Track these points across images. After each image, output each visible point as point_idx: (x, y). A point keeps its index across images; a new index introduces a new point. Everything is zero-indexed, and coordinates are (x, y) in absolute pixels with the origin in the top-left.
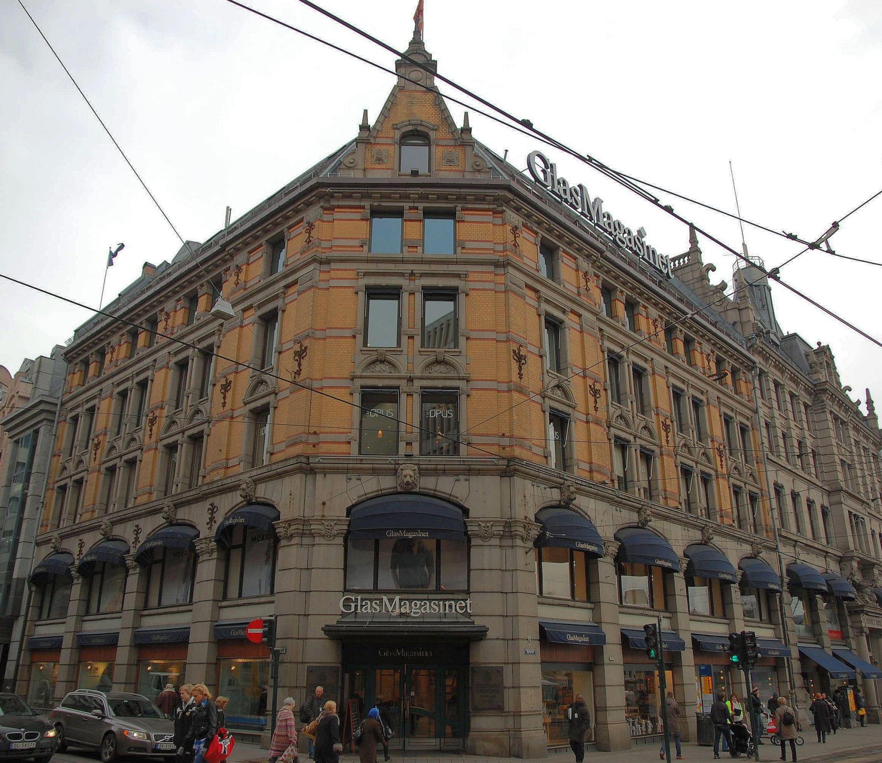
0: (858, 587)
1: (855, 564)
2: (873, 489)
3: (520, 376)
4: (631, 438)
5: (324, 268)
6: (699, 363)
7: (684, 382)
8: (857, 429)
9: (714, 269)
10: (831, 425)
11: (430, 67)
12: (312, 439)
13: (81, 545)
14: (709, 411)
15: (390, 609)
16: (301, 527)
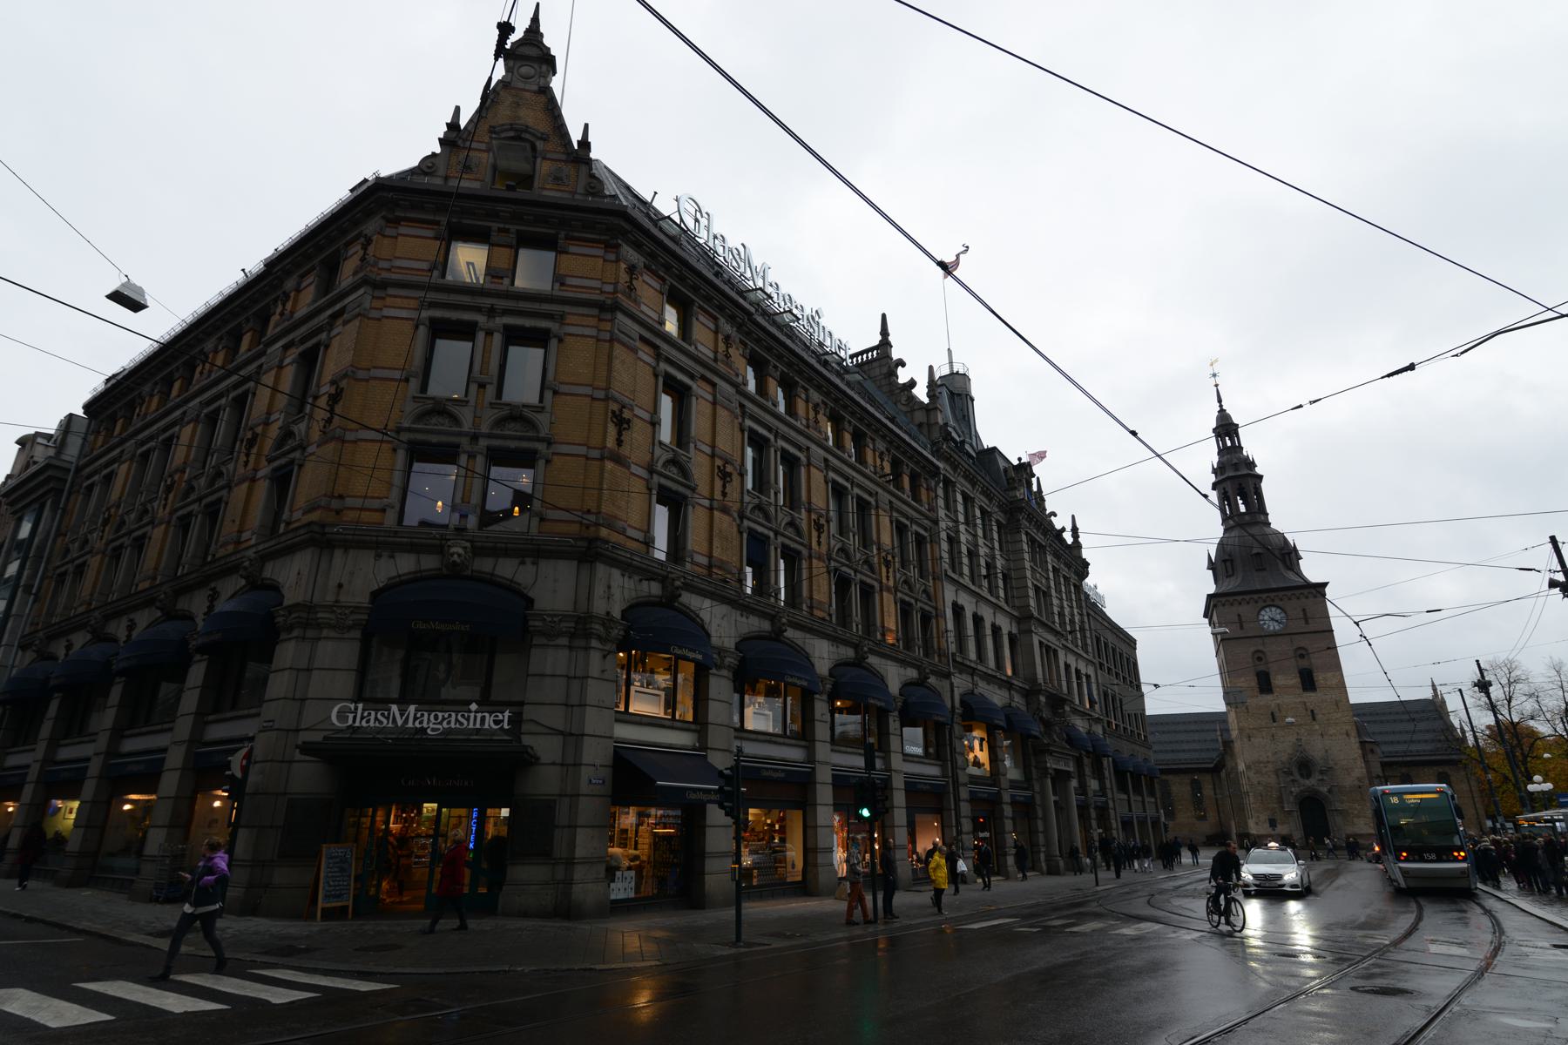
0: (1047, 724)
1: (1043, 699)
2: (1072, 622)
3: (619, 442)
4: (771, 534)
5: (378, 293)
6: (870, 460)
7: (847, 479)
8: (1057, 556)
9: (903, 364)
10: (1025, 547)
11: (547, 62)
12: (335, 504)
13: (69, 647)
14: (878, 515)
15: (400, 722)
16: (304, 615)
